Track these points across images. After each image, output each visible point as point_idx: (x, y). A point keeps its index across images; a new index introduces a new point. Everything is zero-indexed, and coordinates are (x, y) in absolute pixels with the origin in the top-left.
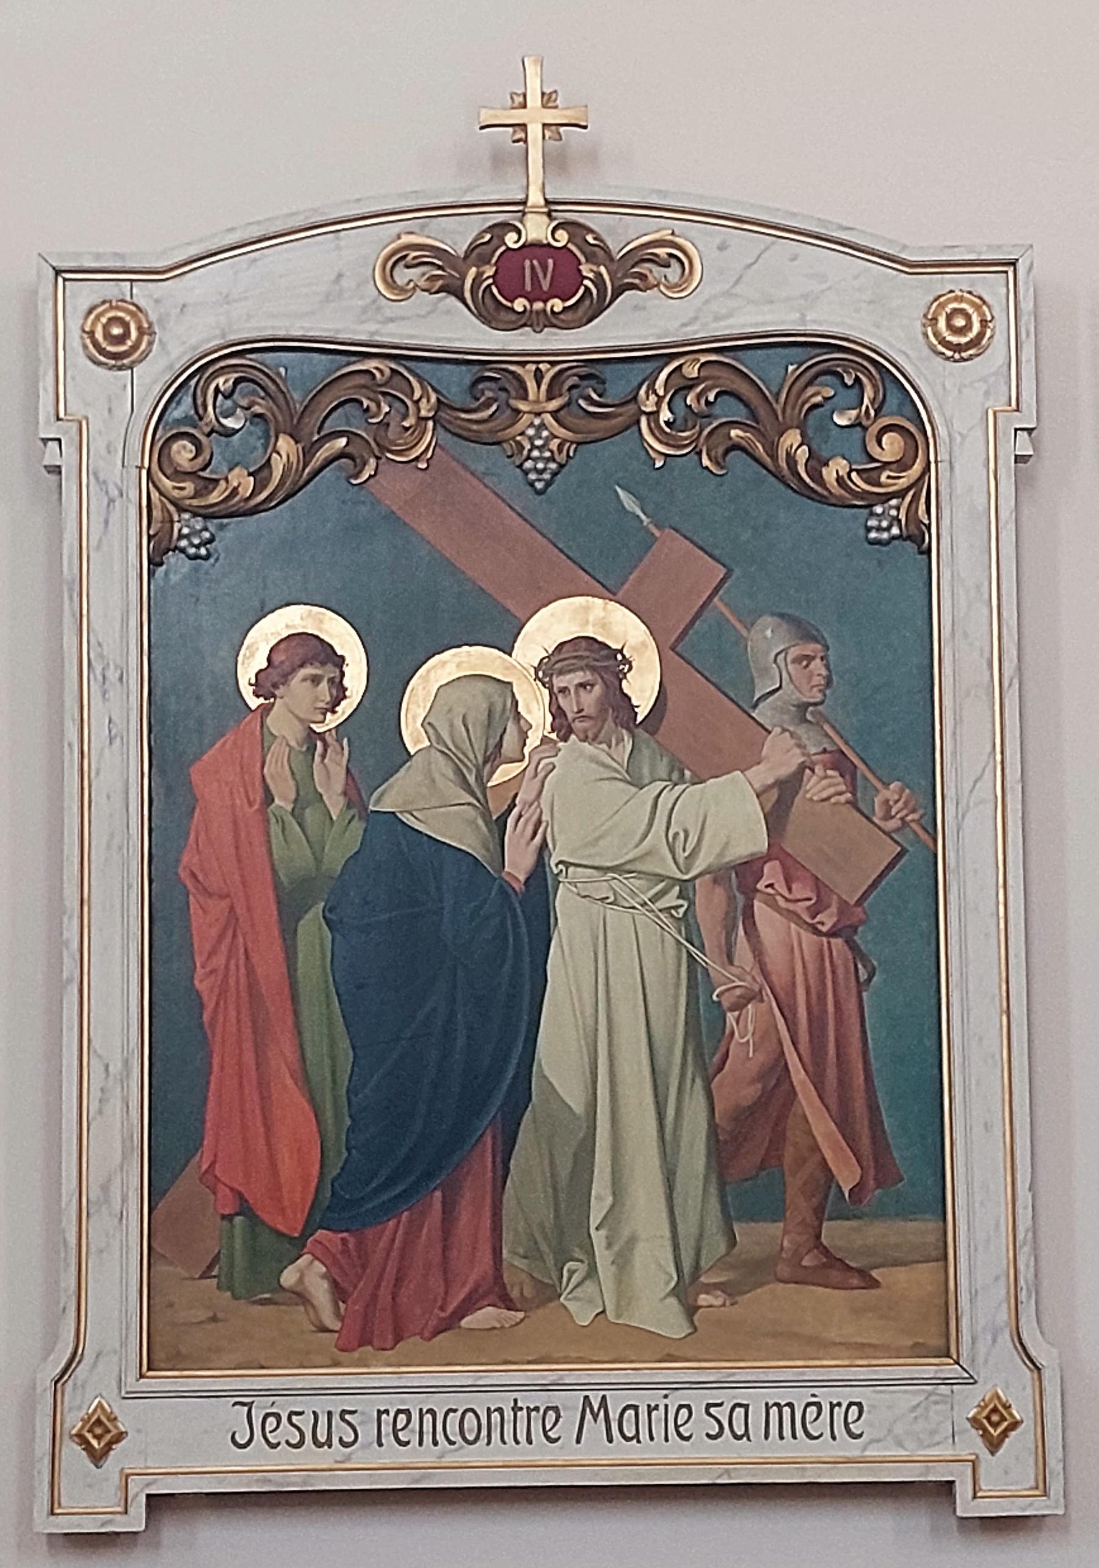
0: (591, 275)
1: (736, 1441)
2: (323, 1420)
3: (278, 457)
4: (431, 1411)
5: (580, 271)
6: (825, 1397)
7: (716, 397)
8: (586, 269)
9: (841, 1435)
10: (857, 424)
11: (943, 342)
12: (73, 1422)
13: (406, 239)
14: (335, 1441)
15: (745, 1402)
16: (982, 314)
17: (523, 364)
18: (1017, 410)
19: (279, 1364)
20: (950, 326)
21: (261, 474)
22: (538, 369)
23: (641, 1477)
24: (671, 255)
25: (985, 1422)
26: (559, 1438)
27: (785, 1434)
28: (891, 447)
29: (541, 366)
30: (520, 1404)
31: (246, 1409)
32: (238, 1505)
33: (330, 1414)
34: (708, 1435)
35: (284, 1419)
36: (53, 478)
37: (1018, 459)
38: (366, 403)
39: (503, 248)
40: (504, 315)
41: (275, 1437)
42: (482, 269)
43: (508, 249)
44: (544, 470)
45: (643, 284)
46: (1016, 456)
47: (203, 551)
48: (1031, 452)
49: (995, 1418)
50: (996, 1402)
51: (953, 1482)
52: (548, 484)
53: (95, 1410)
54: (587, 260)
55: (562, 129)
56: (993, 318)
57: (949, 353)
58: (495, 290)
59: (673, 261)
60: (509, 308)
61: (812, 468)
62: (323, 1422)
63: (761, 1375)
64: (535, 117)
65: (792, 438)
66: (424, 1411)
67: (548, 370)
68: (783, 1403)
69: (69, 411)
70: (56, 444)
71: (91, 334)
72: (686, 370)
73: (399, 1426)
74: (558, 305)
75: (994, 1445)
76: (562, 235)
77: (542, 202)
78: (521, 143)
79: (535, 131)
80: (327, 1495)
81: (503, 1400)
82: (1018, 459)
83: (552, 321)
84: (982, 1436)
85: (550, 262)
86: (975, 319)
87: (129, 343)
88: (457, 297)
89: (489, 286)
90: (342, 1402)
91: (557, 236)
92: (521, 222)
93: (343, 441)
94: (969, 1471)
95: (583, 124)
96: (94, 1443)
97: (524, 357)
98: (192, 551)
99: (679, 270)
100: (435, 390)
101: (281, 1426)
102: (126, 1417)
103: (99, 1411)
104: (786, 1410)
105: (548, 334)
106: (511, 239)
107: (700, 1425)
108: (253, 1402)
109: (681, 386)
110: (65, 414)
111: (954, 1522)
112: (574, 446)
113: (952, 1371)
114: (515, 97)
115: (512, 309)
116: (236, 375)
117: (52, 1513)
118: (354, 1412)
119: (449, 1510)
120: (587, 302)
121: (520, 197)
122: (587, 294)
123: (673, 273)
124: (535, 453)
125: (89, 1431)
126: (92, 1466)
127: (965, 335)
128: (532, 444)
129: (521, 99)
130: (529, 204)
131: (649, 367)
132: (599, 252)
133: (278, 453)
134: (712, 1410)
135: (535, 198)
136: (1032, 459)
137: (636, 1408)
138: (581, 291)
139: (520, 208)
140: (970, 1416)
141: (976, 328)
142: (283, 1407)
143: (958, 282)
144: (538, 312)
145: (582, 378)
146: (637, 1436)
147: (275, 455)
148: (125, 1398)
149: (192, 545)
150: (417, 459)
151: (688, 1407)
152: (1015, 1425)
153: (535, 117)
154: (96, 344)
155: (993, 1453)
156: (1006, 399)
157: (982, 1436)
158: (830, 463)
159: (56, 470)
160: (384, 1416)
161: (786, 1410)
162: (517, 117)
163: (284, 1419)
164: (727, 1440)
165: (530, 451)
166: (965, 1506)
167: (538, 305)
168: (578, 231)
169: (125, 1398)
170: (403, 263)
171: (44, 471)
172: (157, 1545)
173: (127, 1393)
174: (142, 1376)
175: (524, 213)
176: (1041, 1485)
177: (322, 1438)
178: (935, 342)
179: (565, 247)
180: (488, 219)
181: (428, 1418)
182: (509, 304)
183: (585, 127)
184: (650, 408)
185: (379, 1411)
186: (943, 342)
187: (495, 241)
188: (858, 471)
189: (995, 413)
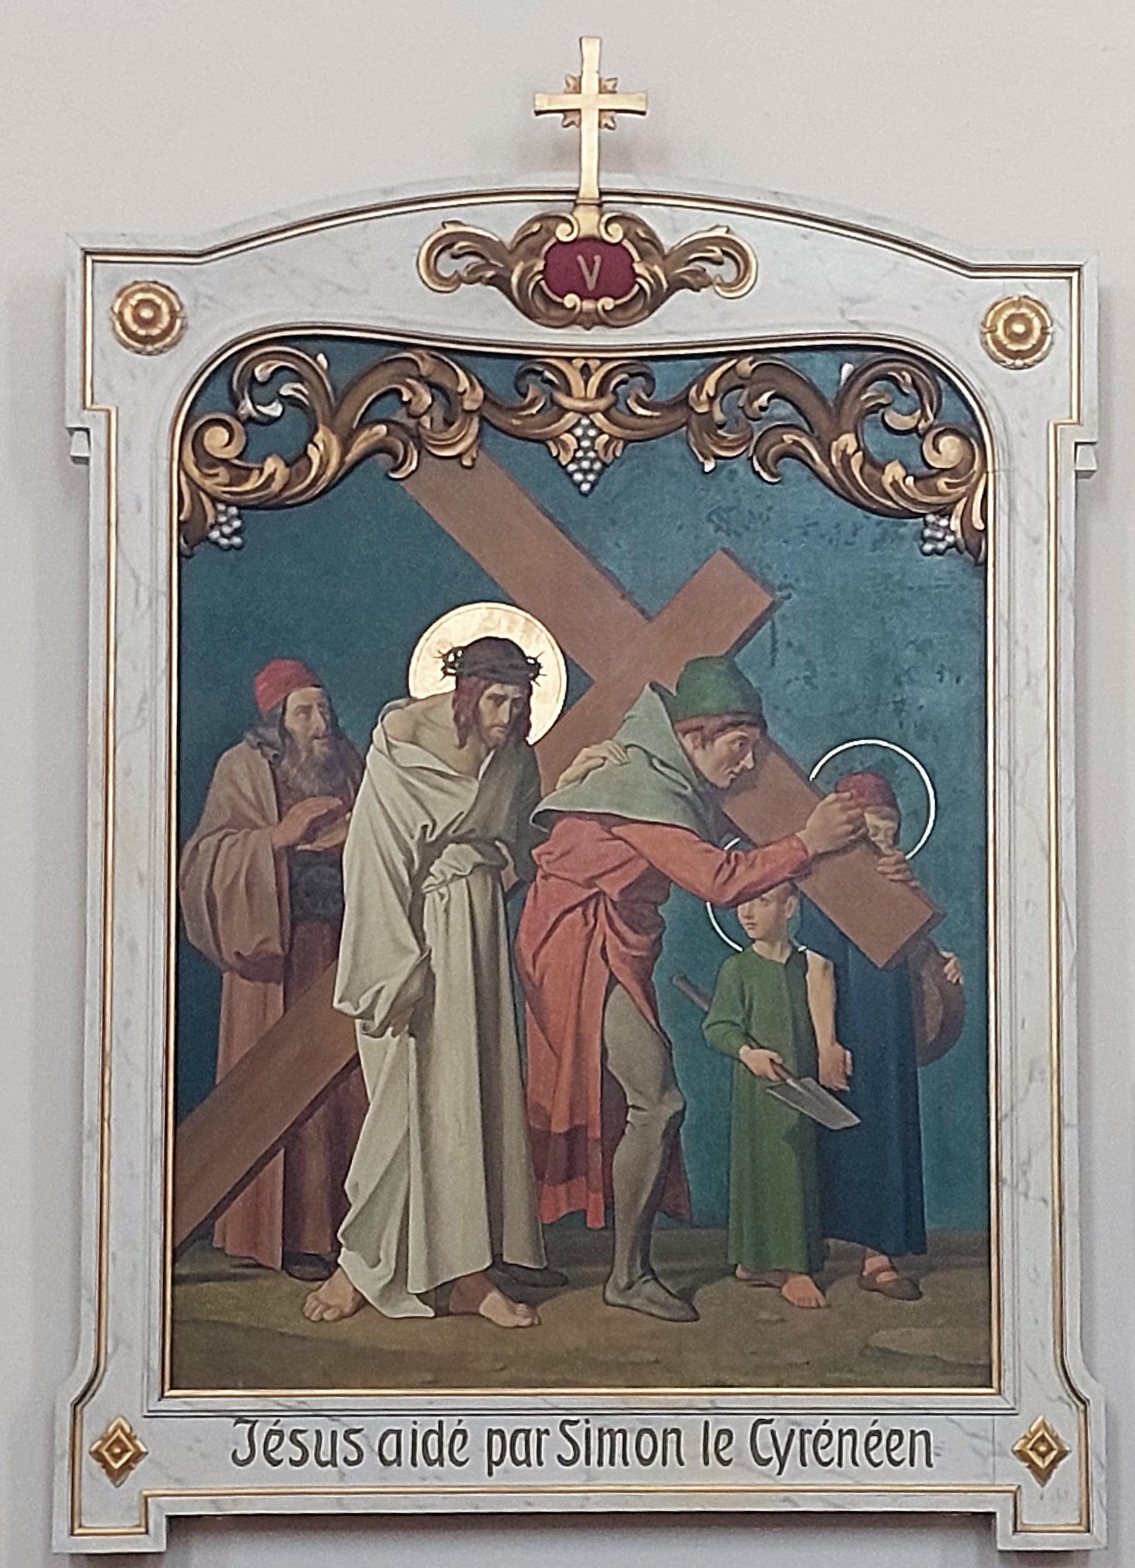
1: (320, 1468)
3: (315, 449)
4: (501, 1433)
5: (633, 269)
6: (405, 1426)
8: (639, 268)
9: (633, 1462)
12: (89, 1441)
13: (451, 229)
14: (339, 1460)
15: (527, 1428)
17: (569, 360)
18: (1079, 423)
19: (661, 1383)
21: (297, 460)
22: (586, 366)
23: (758, 1504)
28: (950, 446)
29: (590, 362)
31: (248, 1426)
34: (559, 1457)
39: (553, 241)
40: (554, 313)
43: (559, 242)
44: (591, 470)
45: (698, 282)
46: (1077, 472)
47: (237, 540)
48: (1094, 468)
50: (119, 1432)
51: (993, 1514)
52: (935, 552)
53: (115, 1431)
57: (1009, 361)
58: (543, 283)
59: (726, 259)
61: (870, 475)
62: (326, 1445)
64: (589, 101)
65: (848, 441)
66: (605, 1430)
67: (597, 369)
68: (917, 1431)
70: (84, 434)
71: (121, 315)
73: (270, 1447)
74: (608, 303)
75: (1043, 1476)
76: (617, 230)
77: (597, 195)
78: (572, 127)
79: (590, 120)
80: (749, 1517)
81: (506, 1423)
85: (597, 258)
86: (1037, 323)
89: (538, 282)
90: (516, 1423)
91: (610, 229)
92: (571, 214)
93: (382, 429)
96: (1038, 1461)
97: (568, 353)
99: (735, 269)
100: (482, 385)
101: (283, 1445)
104: (619, 1436)
107: (475, 1450)
108: (256, 1421)
110: (92, 402)
113: (997, 1402)
114: (612, 83)
117: (72, 1534)
119: (492, 1538)
121: (574, 186)
122: (642, 294)
123: (728, 271)
124: (580, 454)
125: (1031, 1449)
128: (593, 443)
129: (610, 88)
130: (581, 194)
131: (221, 380)
132: (649, 244)
134: (352, 1437)
136: (1095, 475)
137: (677, 1432)
138: (637, 288)
139: (573, 197)
140: (1016, 1448)
141: (1037, 333)
143: (1016, 287)
145: (632, 375)
146: (527, 1461)
147: (310, 446)
148: (146, 1417)
149: (223, 535)
150: (459, 456)
152: (1063, 1454)
153: (589, 101)
155: (1043, 1486)
156: (1068, 414)
158: (888, 468)
160: (807, 1436)
161: (619, 1436)
162: (570, 102)
164: (285, 1467)
165: (576, 451)
168: (633, 226)
169: (146, 1417)
171: (69, 459)
173: (149, 1411)
175: (576, 205)
176: (143, 1523)
179: (619, 243)
182: (559, 300)
183: (643, 113)
184: (703, 409)
185: (490, 1431)
187: (543, 234)
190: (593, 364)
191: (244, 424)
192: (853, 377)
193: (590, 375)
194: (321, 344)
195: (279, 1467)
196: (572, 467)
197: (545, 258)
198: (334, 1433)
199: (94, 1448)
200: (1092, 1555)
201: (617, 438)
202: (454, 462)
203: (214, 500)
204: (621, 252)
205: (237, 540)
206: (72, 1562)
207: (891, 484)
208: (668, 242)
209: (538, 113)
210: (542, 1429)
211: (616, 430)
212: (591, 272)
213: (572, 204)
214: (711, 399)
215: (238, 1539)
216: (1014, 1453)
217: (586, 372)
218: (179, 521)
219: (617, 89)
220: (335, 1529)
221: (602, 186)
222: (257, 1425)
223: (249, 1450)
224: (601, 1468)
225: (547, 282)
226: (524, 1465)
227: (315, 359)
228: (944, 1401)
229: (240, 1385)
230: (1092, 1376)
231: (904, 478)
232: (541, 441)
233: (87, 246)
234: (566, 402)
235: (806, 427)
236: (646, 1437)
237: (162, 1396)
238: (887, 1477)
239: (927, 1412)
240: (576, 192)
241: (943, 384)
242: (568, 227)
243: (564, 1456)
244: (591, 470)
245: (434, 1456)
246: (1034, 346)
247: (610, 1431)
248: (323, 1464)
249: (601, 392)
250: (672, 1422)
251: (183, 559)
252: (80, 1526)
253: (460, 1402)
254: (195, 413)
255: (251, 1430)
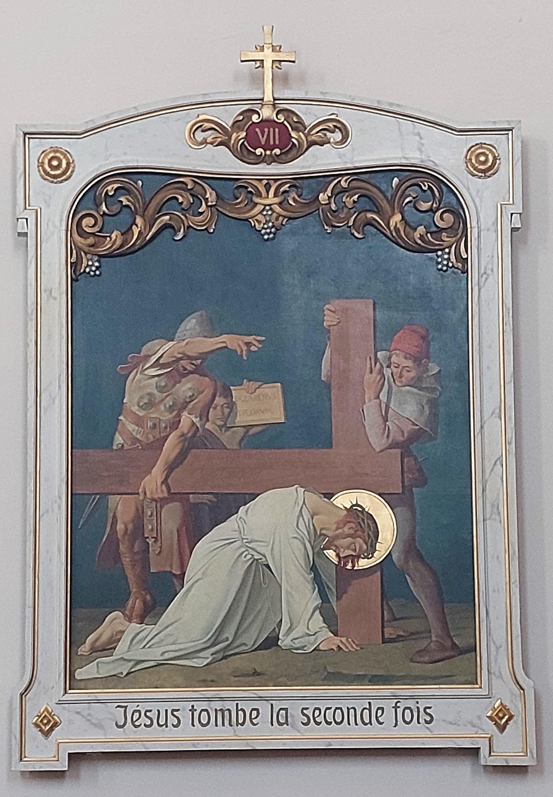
0: (296, 137)
2: (162, 714)
7: (358, 198)
8: (293, 134)
9: (374, 722)
10: (431, 210)
11: (476, 169)
12: (31, 719)
13: (201, 118)
16: (67, 159)
20: (50, 166)
24: (335, 126)
25: (496, 718)
26: (258, 724)
27: (420, 721)
30: (195, 708)
31: (123, 709)
32: (382, 755)
33: (166, 711)
35: (143, 714)
36: (24, 239)
37: (513, 230)
38: (181, 199)
39: (251, 122)
41: (319, 719)
42: (239, 134)
43: (253, 123)
44: (271, 233)
46: (512, 228)
48: (520, 226)
49: (501, 715)
51: (479, 748)
54: (292, 129)
55: (283, 63)
56: (73, 161)
58: (245, 143)
60: (253, 152)
63: (154, 696)
69: (31, 204)
72: (343, 183)
75: (502, 729)
77: (272, 100)
78: (260, 68)
79: (268, 64)
80: (161, 754)
82: (513, 230)
83: (275, 159)
84: (495, 724)
87: (489, 164)
88: (226, 147)
89: (243, 143)
91: (278, 117)
92: (260, 109)
93: (168, 217)
94: (488, 742)
95: (293, 60)
96: (43, 727)
98: (92, 273)
102: (60, 713)
103: (46, 713)
104: (227, 713)
105: (274, 165)
106: (255, 118)
107: (388, 716)
109: (338, 192)
110: (29, 206)
111: (482, 770)
112: (286, 219)
115: (255, 153)
116: (119, 185)
118: (178, 710)
120: (294, 148)
121: (260, 97)
123: (338, 136)
126: (499, 733)
127: (59, 169)
130: (265, 100)
131: (91, 194)
132: (299, 125)
133: (137, 226)
135: (268, 97)
136: (520, 230)
138: (291, 143)
141: (64, 165)
142: (143, 707)
144: (269, 155)
151: (257, 710)
153: (268, 56)
154: (473, 165)
157: (495, 724)
159: (26, 234)
162: (258, 56)
163: (143, 714)
166: (484, 759)
167: (268, 152)
168: (291, 115)
170: (200, 129)
172: (78, 777)
174: (481, 688)
175: (263, 105)
177: (162, 722)
178: (472, 170)
179: (283, 123)
180: (242, 108)
181: (352, 711)
183: (294, 62)
186: (476, 169)
188: (431, 233)
189: (501, 205)
190: (272, 182)
191: (102, 215)
192: (399, 186)
193: (270, 187)
194: (139, 176)
195: (139, 728)
196: (263, 231)
197: (246, 131)
198: (166, 711)
199: (34, 721)
200: (529, 769)
201: (281, 215)
202: (206, 231)
203: (86, 253)
204: (283, 127)
205: (98, 273)
206: (21, 774)
207: (420, 239)
208: (309, 121)
209: (242, 61)
210: (350, 707)
211: (284, 213)
212: (263, 137)
213: (260, 105)
214: (329, 198)
215: (181, 764)
216: (33, 723)
217: (268, 187)
218: (71, 262)
219: (281, 50)
220: (123, 759)
221: (275, 96)
222: (128, 707)
223: (175, 719)
224: (218, 727)
225: (247, 143)
226: (369, 725)
227: (136, 183)
228: (369, 693)
229: (101, 687)
230: (528, 677)
231: (426, 234)
232: (247, 220)
233: (26, 130)
234: (257, 200)
235: (376, 210)
236: (407, 711)
237: (66, 692)
238: (143, 733)
239: (433, 697)
240: (262, 100)
241: (444, 189)
242: (257, 116)
243: (304, 722)
244: (271, 233)
245: (162, 722)
246: (490, 166)
247: (221, 710)
248: (366, 724)
249: (275, 195)
250: (256, 705)
251: (74, 282)
252: (494, 752)
253: (414, 692)
254: (79, 209)
255: (125, 712)
